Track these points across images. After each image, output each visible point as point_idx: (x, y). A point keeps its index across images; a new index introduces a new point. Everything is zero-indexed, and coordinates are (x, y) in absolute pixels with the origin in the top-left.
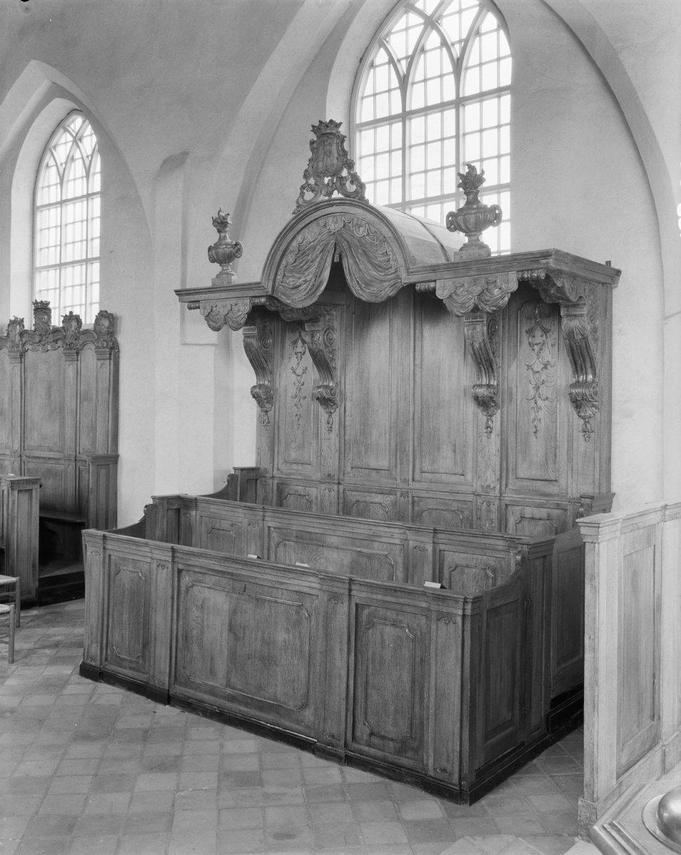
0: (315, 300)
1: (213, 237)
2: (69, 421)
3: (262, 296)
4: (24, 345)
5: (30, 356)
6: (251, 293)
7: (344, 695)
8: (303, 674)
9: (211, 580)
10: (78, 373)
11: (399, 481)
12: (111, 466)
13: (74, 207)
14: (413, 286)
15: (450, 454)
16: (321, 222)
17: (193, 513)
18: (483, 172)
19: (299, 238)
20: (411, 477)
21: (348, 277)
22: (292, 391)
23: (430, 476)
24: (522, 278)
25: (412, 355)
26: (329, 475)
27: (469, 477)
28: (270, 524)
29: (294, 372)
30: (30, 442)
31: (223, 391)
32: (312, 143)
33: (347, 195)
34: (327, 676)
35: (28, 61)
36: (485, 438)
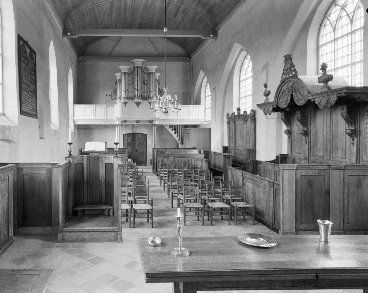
0: (287, 106)
1: (264, 89)
2: (245, 140)
3: (275, 105)
4: (235, 119)
5: (237, 122)
6: (272, 104)
7: (272, 212)
8: (265, 206)
9: (249, 180)
10: (246, 127)
11: (325, 160)
12: (254, 152)
13: (348, 38)
14: (310, 100)
15: (341, 152)
16: (288, 83)
17: (260, 165)
18: (327, 64)
19: (283, 88)
20: (329, 159)
21: (294, 99)
22: (296, 131)
23: (335, 159)
24: (338, 96)
25: (329, 119)
26: (306, 157)
27: (347, 159)
28: (276, 169)
29: (297, 126)
30: (237, 146)
31: (278, 130)
32: (285, 61)
33: (293, 75)
34: (269, 207)
35: (235, 43)
36: (352, 147)
